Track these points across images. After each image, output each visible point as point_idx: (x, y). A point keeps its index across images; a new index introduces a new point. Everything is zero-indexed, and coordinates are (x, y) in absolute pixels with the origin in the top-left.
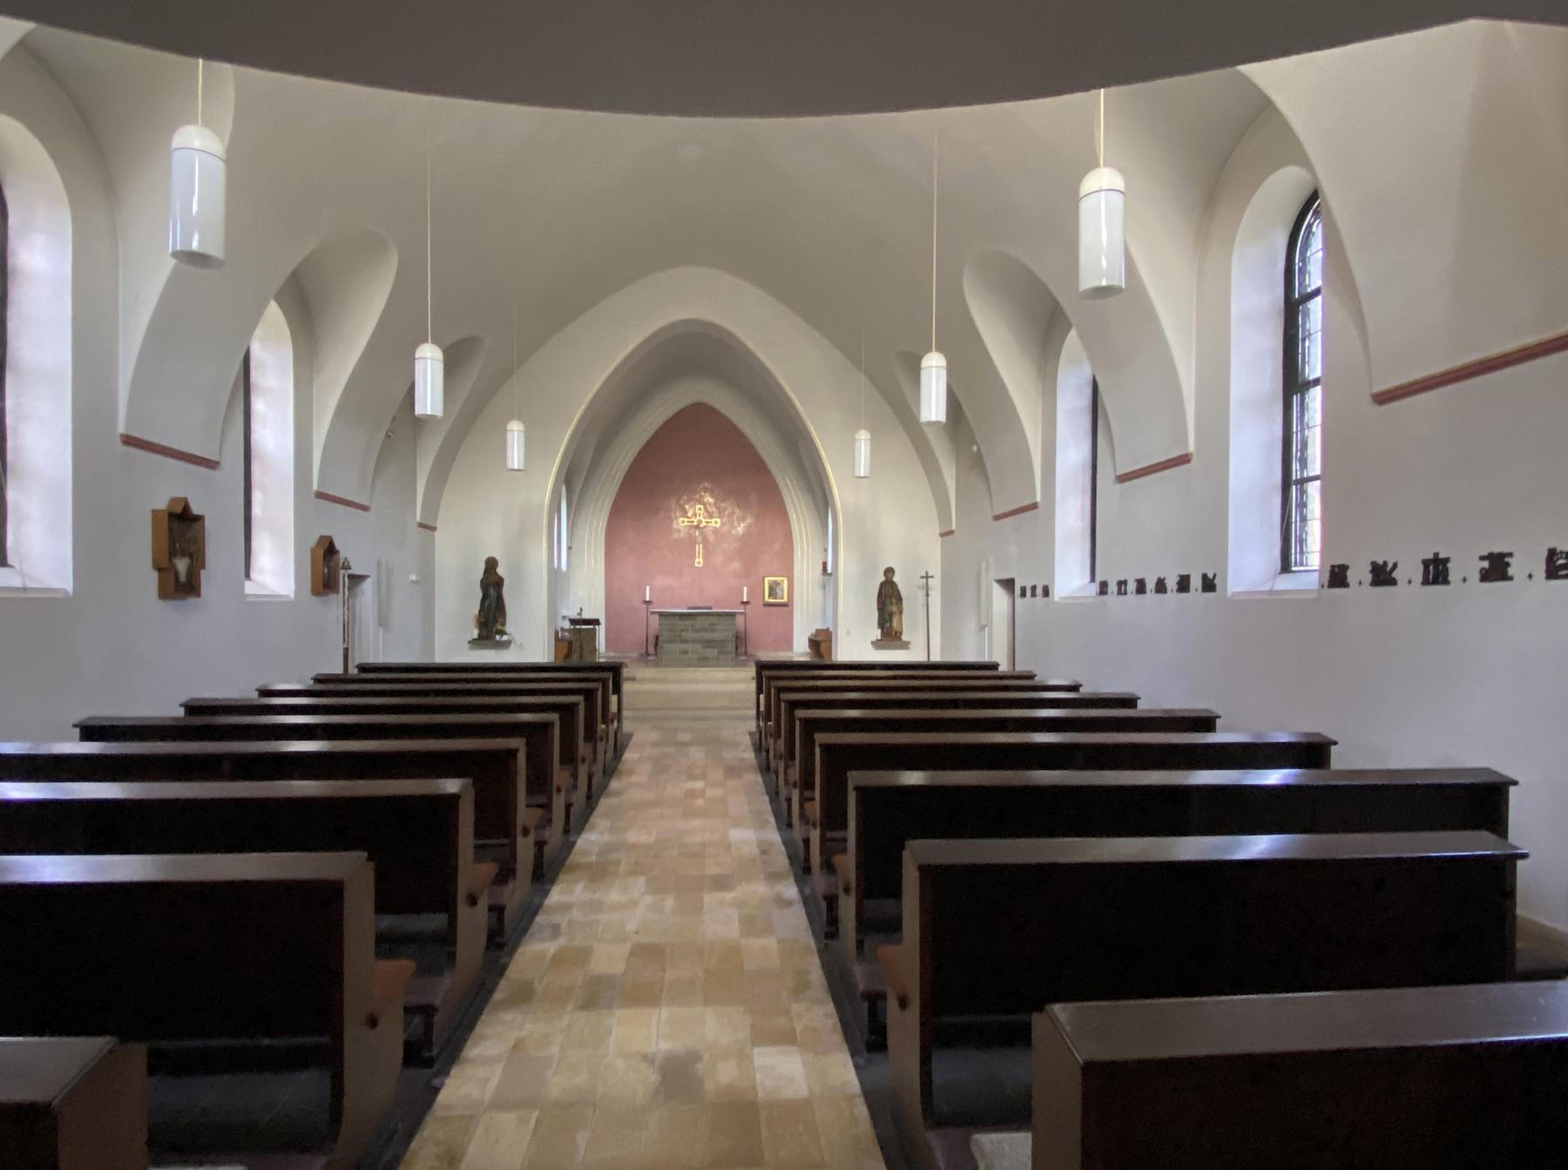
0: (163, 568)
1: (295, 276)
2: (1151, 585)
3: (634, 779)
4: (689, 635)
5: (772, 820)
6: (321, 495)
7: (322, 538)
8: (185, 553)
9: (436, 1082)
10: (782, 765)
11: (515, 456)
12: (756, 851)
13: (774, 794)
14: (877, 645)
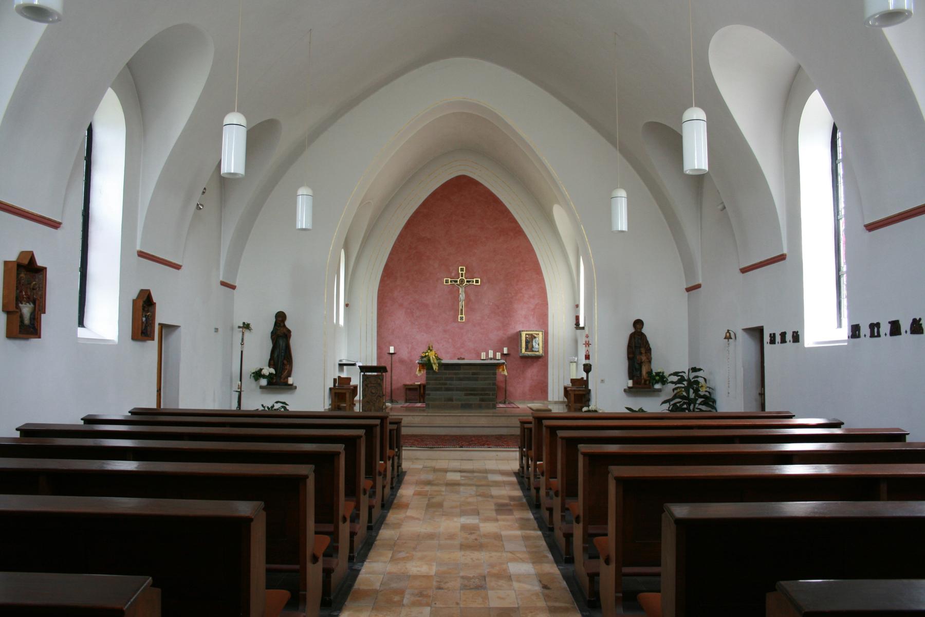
0: (11, 312)
1: (129, 65)
2: (905, 326)
3: (410, 513)
4: (456, 383)
5: (550, 556)
6: (142, 254)
7: (142, 291)
8: (30, 300)
9: (356, 567)
10: (557, 502)
11: (303, 219)
12: (537, 588)
13: (547, 528)
14: (629, 391)
